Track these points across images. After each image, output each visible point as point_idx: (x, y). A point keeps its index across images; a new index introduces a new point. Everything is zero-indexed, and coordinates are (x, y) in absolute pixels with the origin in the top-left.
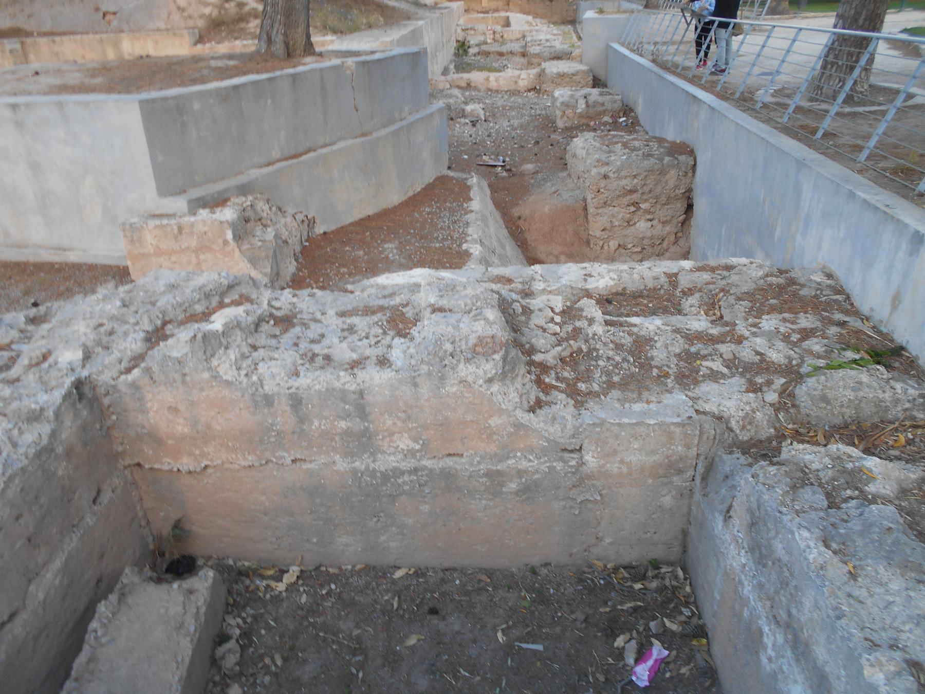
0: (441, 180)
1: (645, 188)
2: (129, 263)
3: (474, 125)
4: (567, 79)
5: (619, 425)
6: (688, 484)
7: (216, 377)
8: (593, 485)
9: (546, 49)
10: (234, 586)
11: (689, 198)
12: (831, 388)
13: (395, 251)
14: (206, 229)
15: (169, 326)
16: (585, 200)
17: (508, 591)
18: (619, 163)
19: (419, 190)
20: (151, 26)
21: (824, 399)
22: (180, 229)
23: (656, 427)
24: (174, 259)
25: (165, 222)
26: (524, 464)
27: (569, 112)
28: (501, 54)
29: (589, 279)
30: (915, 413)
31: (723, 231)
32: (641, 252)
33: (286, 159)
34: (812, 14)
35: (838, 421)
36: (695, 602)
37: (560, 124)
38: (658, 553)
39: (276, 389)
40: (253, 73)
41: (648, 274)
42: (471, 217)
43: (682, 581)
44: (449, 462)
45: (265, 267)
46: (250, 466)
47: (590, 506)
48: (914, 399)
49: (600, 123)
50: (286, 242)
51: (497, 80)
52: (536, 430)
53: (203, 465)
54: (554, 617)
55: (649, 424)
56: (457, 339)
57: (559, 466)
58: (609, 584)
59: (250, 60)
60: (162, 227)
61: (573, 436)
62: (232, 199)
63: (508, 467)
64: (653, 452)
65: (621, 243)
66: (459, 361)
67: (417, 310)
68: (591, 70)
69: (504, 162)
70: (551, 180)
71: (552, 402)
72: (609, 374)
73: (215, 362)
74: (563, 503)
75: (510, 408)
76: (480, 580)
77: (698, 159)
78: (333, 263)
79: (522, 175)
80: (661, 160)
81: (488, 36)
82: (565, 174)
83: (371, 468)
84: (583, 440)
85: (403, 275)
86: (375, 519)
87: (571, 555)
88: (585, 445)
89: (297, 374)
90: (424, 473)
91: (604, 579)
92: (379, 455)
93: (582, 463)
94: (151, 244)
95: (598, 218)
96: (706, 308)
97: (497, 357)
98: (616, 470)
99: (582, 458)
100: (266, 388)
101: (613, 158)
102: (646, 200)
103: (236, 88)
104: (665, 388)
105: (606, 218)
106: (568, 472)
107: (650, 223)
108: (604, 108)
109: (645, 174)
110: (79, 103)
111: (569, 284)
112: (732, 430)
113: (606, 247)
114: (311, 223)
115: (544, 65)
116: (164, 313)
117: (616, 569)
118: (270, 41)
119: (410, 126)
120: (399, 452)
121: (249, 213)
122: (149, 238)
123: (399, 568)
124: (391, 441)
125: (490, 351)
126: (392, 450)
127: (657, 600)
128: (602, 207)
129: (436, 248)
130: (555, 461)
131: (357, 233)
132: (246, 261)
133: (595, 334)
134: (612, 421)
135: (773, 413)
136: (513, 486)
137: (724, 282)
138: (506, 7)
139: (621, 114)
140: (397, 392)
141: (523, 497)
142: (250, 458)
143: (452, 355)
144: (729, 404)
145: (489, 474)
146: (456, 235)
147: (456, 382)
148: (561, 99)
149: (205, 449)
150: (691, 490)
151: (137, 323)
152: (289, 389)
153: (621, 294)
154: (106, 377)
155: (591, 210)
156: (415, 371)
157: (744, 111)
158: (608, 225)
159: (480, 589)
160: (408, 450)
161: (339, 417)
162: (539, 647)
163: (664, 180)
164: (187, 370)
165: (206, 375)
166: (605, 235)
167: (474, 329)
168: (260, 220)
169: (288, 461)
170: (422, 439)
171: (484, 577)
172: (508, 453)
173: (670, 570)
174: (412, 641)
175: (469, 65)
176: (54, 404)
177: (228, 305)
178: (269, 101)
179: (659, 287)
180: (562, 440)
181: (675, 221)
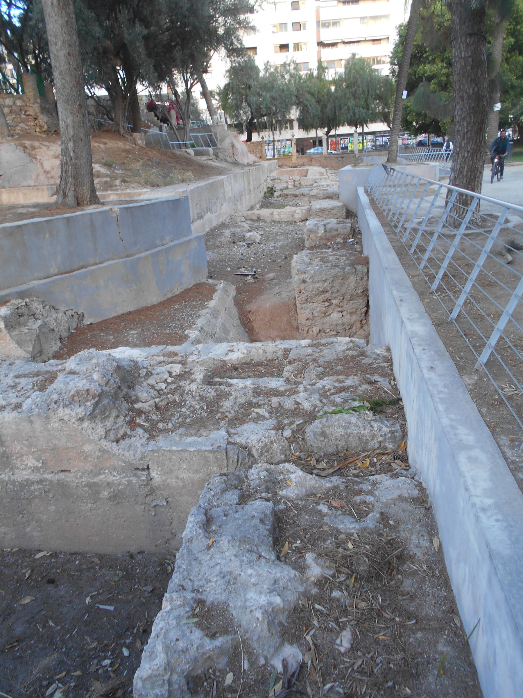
0: (198, 286)
1: (333, 289)
3: (248, 247)
5: (170, 451)
8: (162, 495)
9: (321, 192)
12: (329, 427)
17: (109, 570)
18: (312, 272)
20: (25, 184)
21: (324, 434)
26: (111, 479)
27: (312, 236)
28: (296, 196)
30: (387, 444)
34: (518, 163)
35: (331, 450)
44: (62, 476)
45: (28, 347)
48: (385, 435)
49: (335, 243)
50: (53, 330)
51: (279, 214)
54: (131, 588)
59: (47, 208)
61: (141, 459)
64: (197, 471)
66: (59, 406)
72: (185, 418)
74: (143, 507)
75: (96, 439)
80: (343, 269)
86: (21, 515)
87: (157, 546)
92: (16, 470)
95: (303, 311)
102: (335, 298)
105: (308, 311)
107: (341, 314)
108: (337, 232)
109: (332, 279)
113: (310, 332)
119: (168, 250)
121: (24, 310)
126: (23, 467)
129: (166, 334)
131: (115, 324)
135: (287, 444)
138: (310, 163)
140: (20, 427)
141: (115, 502)
143: (56, 403)
145: (89, 485)
158: (310, 316)
159: (91, 568)
162: (111, 608)
163: (347, 283)
166: (309, 323)
168: (33, 315)
172: (100, 470)
174: (27, 600)
175: (271, 204)
178: (47, 235)
180: (134, 462)
181: (359, 312)
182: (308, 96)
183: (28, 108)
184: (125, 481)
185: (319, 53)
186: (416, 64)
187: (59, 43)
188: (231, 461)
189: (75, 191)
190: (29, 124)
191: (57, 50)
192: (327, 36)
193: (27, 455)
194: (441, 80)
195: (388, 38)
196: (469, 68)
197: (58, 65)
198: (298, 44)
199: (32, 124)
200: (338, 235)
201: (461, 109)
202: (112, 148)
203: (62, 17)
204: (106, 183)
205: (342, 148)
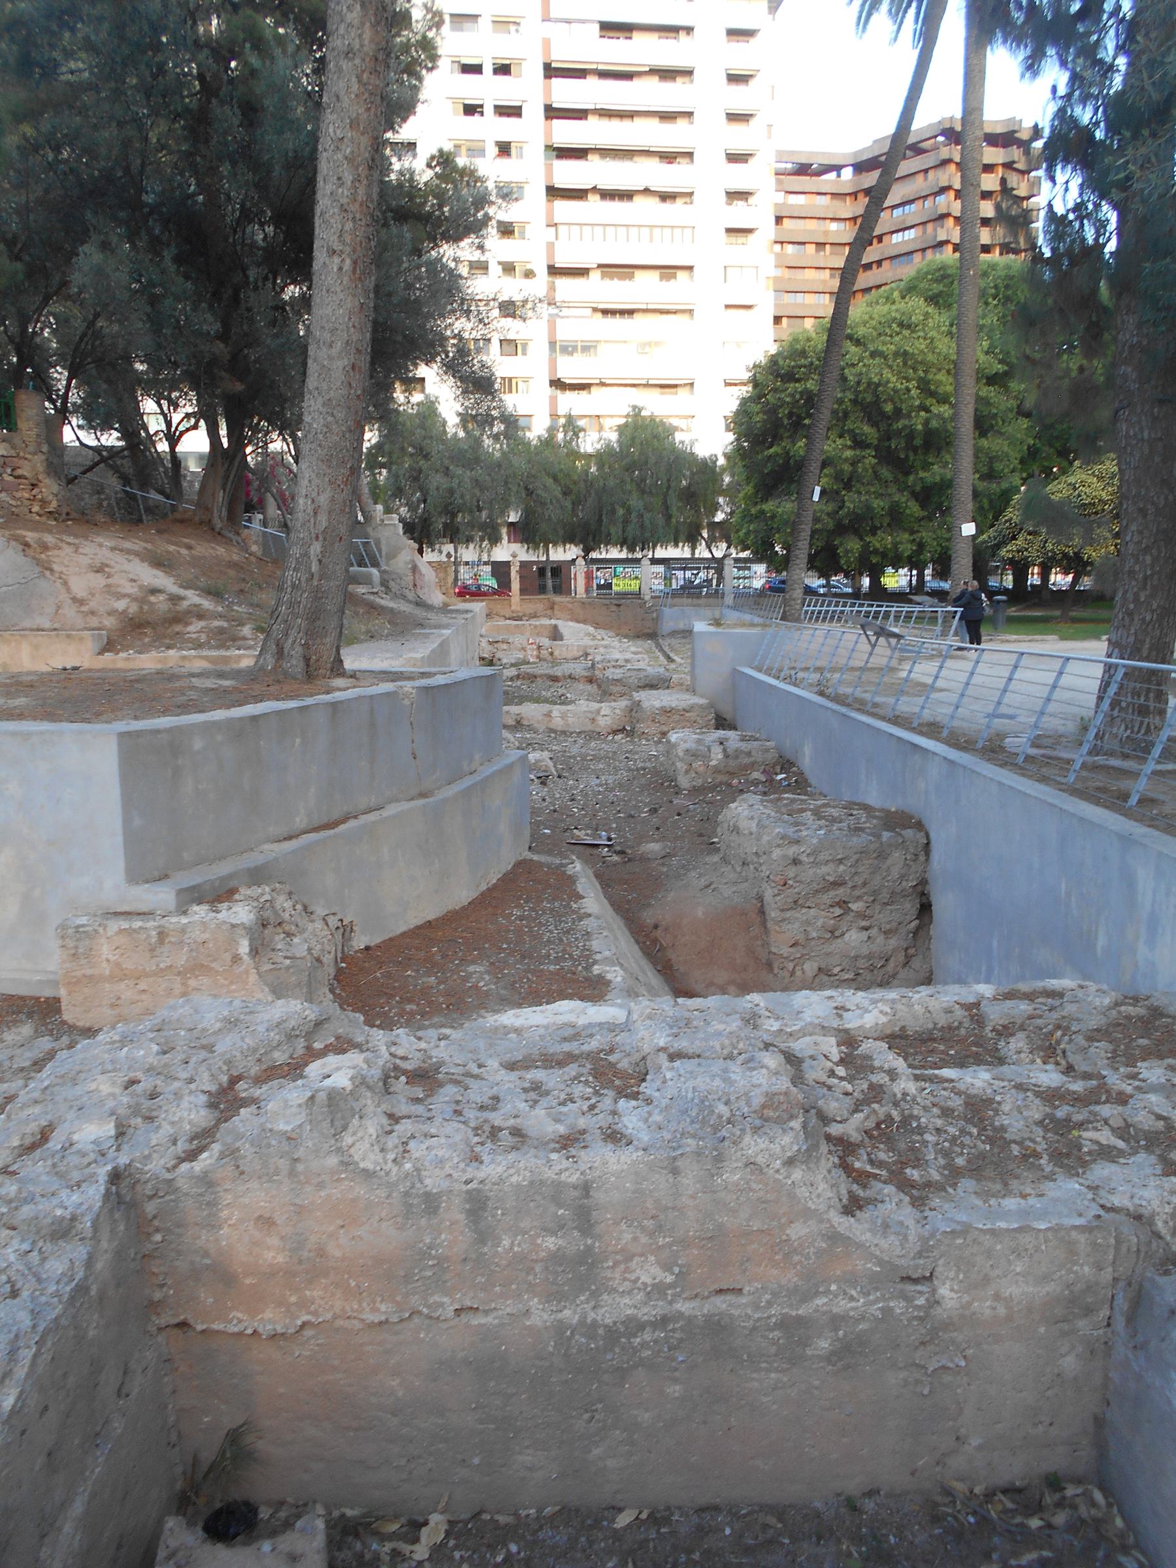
0: (522, 866)
1: (856, 878)
2: (63, 993)
3: (544, 783)
4: (677, 717)
5: (993, 1232)
6: (1101, 1332)
7: (347, 1164)
8: (953, 1341)
10: (337, 1554)
11: (923, 894)
13: (487, 977)
14: (206, 936)
15: (241, 1085)
16: (760, 899)
18: (815, 841)
19: (494, 881)
20: (27, 623)
22: (162, 935)
23: (1050, 1234)
24: (142, 986)
25: (137, 924)
26: (842, 1305)
27: (698, 764)
28: (555, 679)
29: (845, 1014)
31: (995, 943)
32: (853, 980)
33: (316, 829)
36: (1137, 1546)
37: (684, 782)
38: (1056, 1461)
39: (445, 1184)
40: (269, 700)
41: (934, 1005)
42: (589, 924)
43: (1105, 1509)
44: (720, 1303)
46: (381, 1323)
47: (947, 1378)
49: (747, 781)
51: (563, 716)
52: (860, 1246)
53: (299, 1323)
55: (1040, 1230)
56: (733, 1098)
57: (898, 1306)
58: (984, 1520)
60: (130, 932)
61: (919, 1255)
62: (243, 890)
63: (816, 1311)
64: (1046, 1278)
65: (823, 966)
66: (743, 1130)
67: (636, 1057)
68: (712, 705)
69: (609, 839)
70: (695, 868)
71: (876, 1199)
73: (348, 1139)
74: (902, 1375)
75: (822, 1208)
76: (766, 1526)
77: (933, 836)
78: (392, 996)
79: (644, 859)
81: (529, 652)
82: (716, 858)
83: (589, 1321)
84: (936, 1261)
85: (541, 1011)
86: (586, 1416)
88: (939, 1269)
89: (476, 1159)
90: (678, 1325)
91: (974, 1513)
92: (605, 1297)
93: (934, 1302)
94: (108, 960)
95: (785, 927)
96: (1042, 1054)
97: (796, 1124)
98: (988, 1312)
99: (934, 1291)
100: (428, 1181)
101: (804, 833)
102: (859, 898)
103: (254, 719)
104: (1040, 1173)
105: (797, 925)
106: (915, 1318)
107: (865, 934)
109: (857, 856)
110: (14, 734)
111: (817, 1021)
112: (1159, 1236)
113: (798, 973)
114: (346, 930)
115: (637, 696)
116: (229, 1063)
117: (989, 1496)
118: (280, 653)
120: (639, 1289)
122: (105, 951)
123: (621, 1510)
124: (627, 1270)
125: (785, 1116)
126: (627, 1285)
127: (1072, 1545)
128: (791, 908)
130: (891, 1298)
132: (267, 989)
133: (905, 1094)
134: (981, 1226)
136: (824, 1345)
137: (1055, 1015)
138: (549, 612)
139: (778, 769)
141: (839, 1365)
142: (383, 1308)
144: (1146, 1193)
145: (785, 1324)
146: (576, 953)
147: (740, 1165)
148: (684, 746)
149: (308, 1293)
150: (1106, 1343)
151: (191, 1080)
152: (467, 1182)
153: (900, 1037)
154: (156, 1166)
155: (773, 914)
156: (674, 1149)
157: (1001, 766)
159: (770, 1542)
160: (653, 1285)
161: (544, 1229)
163: (884, 867)
164: (300, 1153)
165: (333, 1161)
166: (797, 953)
167: (755, 1081)
169: (450, 1312)
170: (678, 1265)
171: (772, 1520)
173: (1079, 1491)
176: (90, 1208)
177: (323, 1053)
178: (298, 741)
179: (956, 1024)
180: (903, 1262)
182: (549, 482)
183: (22, 462)
184: (875, 1310)
185: (553, 402)
186: (789, 437)
187: (339, 345)
188: (1124, 1249)
189: (306, 646)
190: (18, 495)
191: (330, 358)
192: (569, 370)
193: (641, 1255)
194: (842, 471)
195: (692, 384)
196: (1157, 459)
197: (325, 386)
198: (510, 379)
199: (26, 495)
200: (753, 764)
201: (1140, 532)
202: (205, 557)
203: (354, 296)
204: (221, 631)
205: (599, 587)
